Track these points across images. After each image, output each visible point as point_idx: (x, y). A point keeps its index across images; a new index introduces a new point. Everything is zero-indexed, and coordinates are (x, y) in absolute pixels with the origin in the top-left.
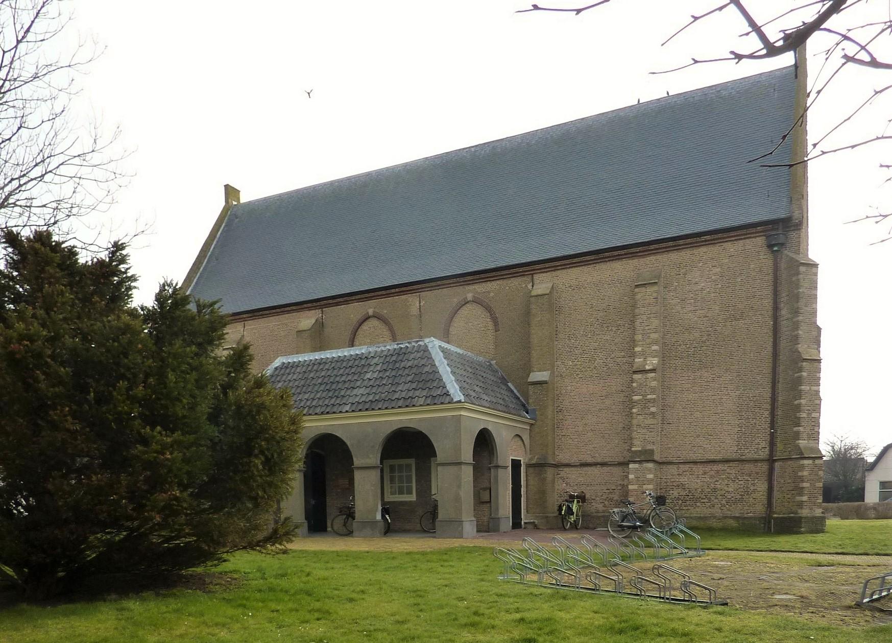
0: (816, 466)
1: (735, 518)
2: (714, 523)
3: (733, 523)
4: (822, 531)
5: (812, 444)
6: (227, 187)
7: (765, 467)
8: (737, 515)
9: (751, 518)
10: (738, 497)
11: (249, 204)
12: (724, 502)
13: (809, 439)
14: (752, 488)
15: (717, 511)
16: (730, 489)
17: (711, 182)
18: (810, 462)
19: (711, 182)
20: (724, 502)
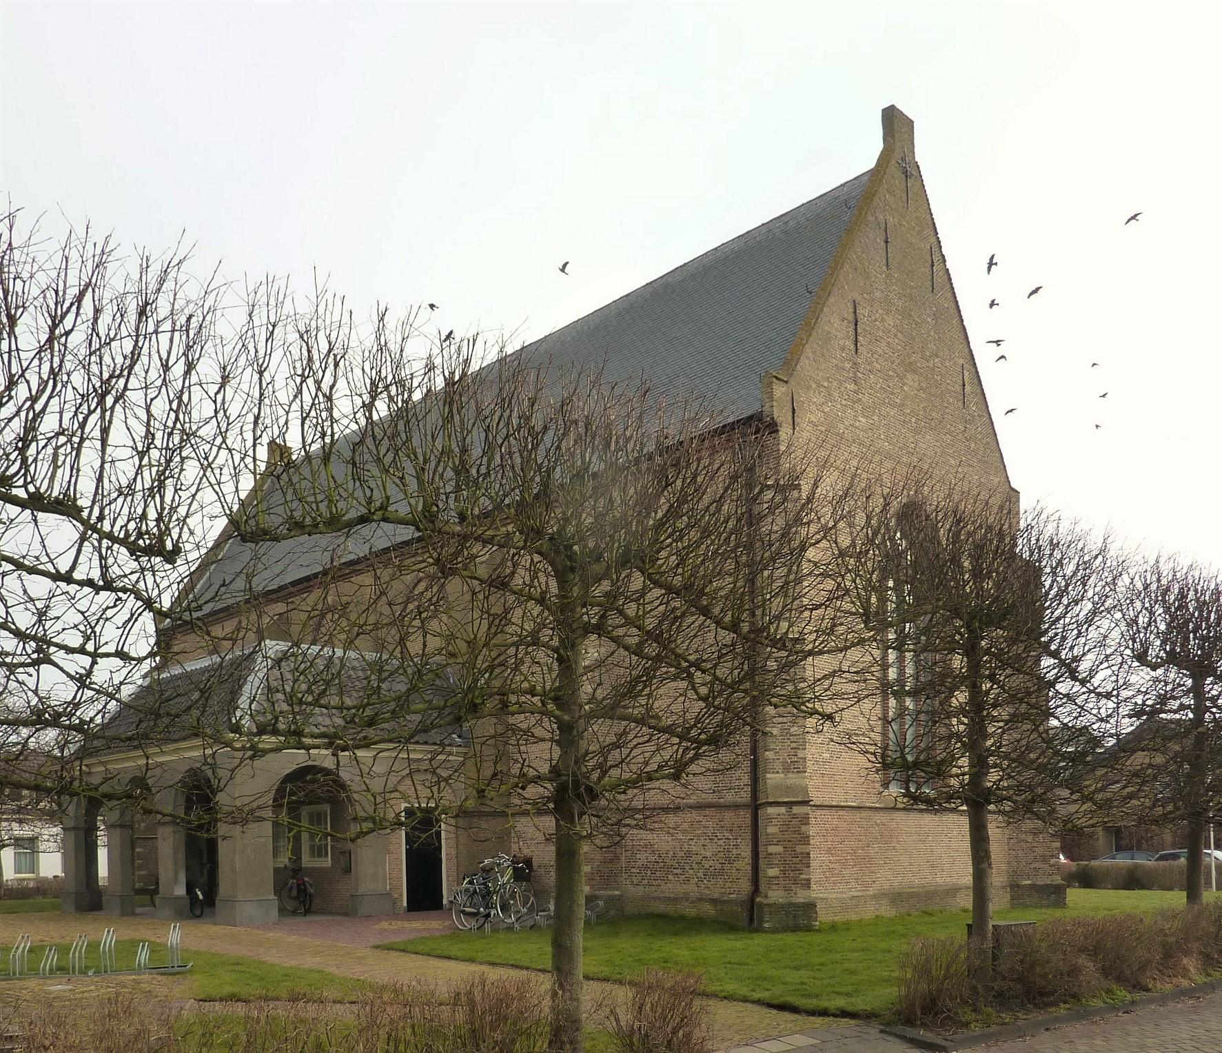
0: (795, 816)
1: (713, 901)
2: (689, 910)
3: (708, 910)
4: (809, 929)
5: (793, 779)
6: (451, 332)
7: (745, 817)
8: (716, 896)
9: (731, 901)
10: (718, 866)
11: (65, 870)
12: (700, 875)
13: (786, 769)
14: (735, 852)
15: (692, 889)
16: (709, 854)
17: (860, 248)
18: (783, 810)
19: (860, 248)
20: (700, 875)
